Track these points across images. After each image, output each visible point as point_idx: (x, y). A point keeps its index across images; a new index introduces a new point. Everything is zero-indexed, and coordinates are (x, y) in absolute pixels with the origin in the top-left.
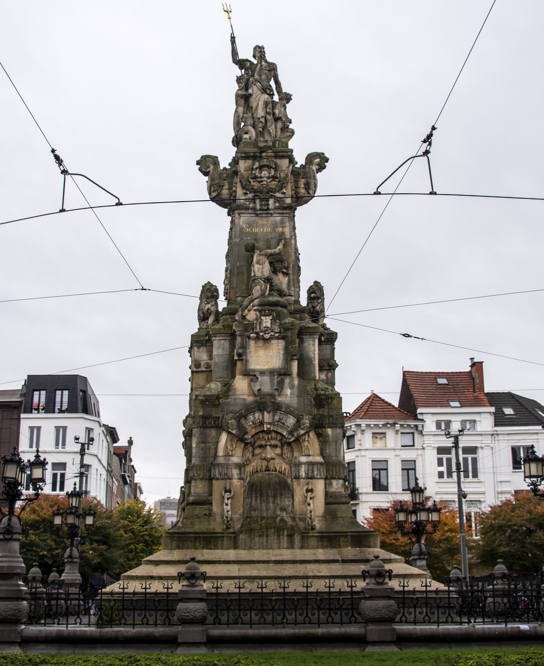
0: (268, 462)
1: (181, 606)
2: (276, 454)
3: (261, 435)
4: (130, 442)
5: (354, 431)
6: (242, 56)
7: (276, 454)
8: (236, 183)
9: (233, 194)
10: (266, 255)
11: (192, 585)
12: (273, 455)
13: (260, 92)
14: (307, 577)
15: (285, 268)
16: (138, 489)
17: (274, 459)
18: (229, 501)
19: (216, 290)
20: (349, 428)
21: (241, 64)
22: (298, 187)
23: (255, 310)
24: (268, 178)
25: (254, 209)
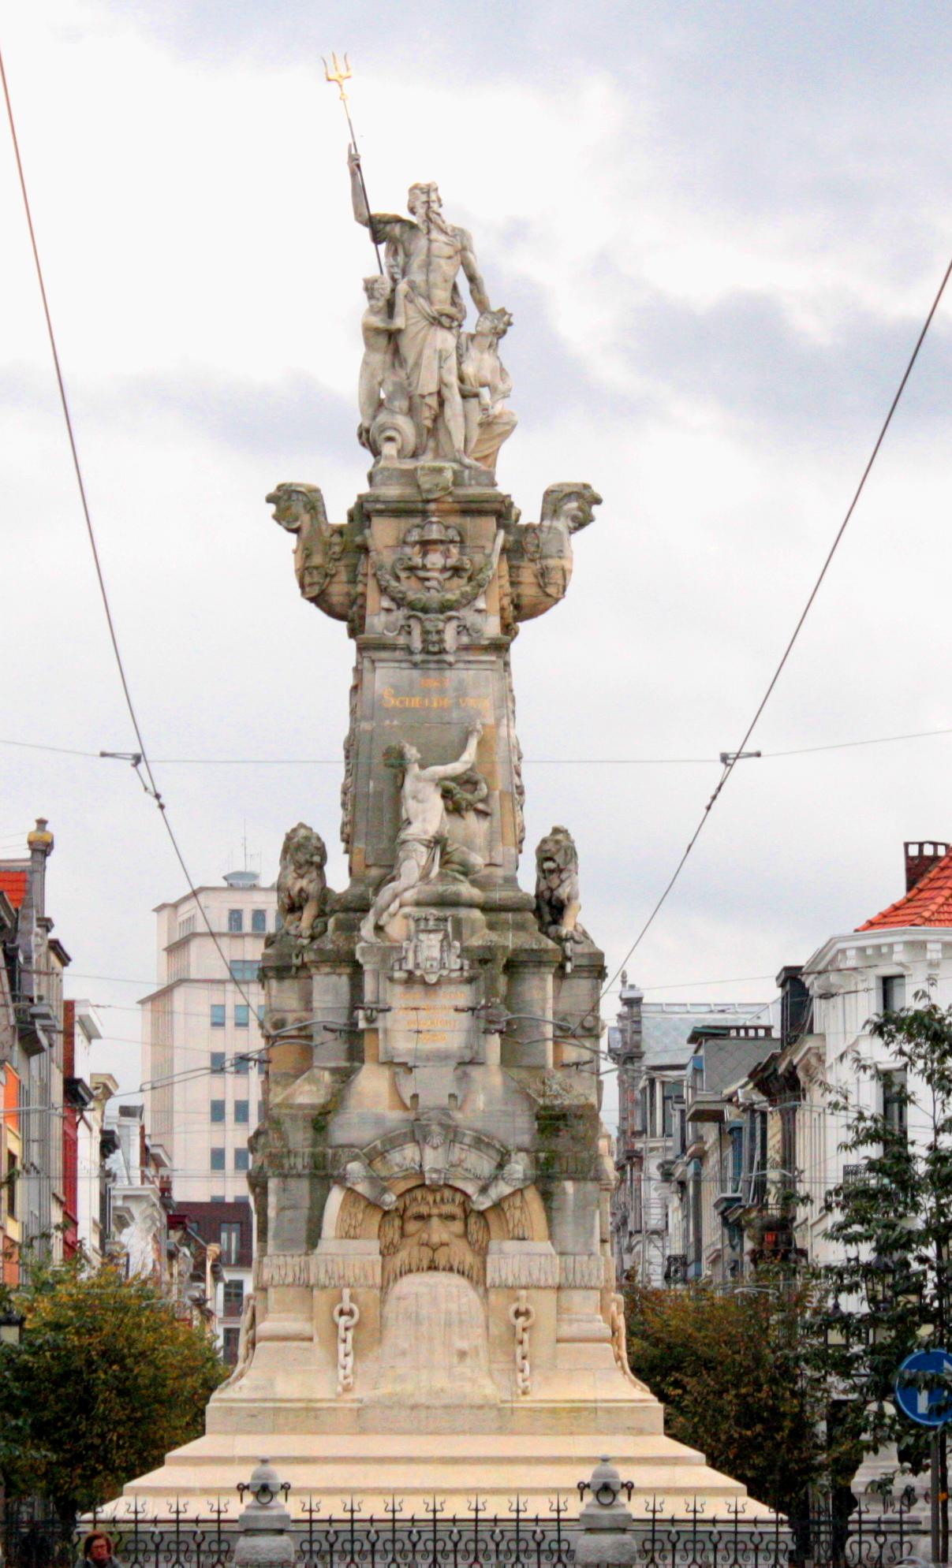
0: (434, 1250)
1: (243, 1543)
2: (451, 1233)
3: (418, 1194)
4: (42, 848)
5: (900, 964)
6: (377, 208)
7: (451, 1233)
8: (366, 575)
9: (359, 602)
10: (432, 780)
11: (264, 1506)
12: (445, 1237)
13: (424, 323)
15: (483, 801)
16: (78, 1030)
17: (447, 1245)
18: (350, 1335)
19: (322, 851)
20: (884, 950)
21: (379, 228)
22: (519, 583)
23: (406, 917)
24: (444, 569)
25: (409, 650)
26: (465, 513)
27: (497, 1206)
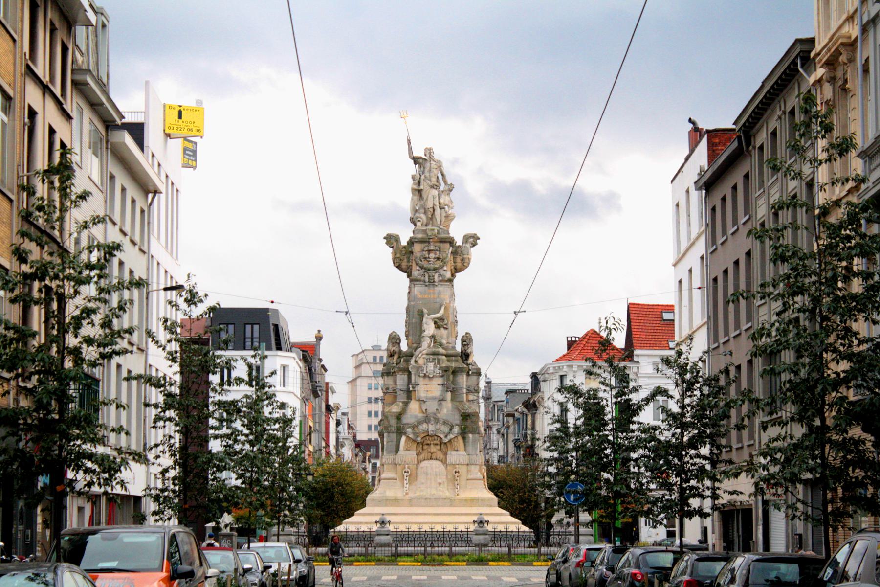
1: (377, 538)
14: (408, 523)
19: (399, 339)
21: (416, 160)
25: (424, 281)
26: (441, 242)
27: (450, 441)
